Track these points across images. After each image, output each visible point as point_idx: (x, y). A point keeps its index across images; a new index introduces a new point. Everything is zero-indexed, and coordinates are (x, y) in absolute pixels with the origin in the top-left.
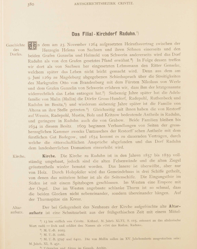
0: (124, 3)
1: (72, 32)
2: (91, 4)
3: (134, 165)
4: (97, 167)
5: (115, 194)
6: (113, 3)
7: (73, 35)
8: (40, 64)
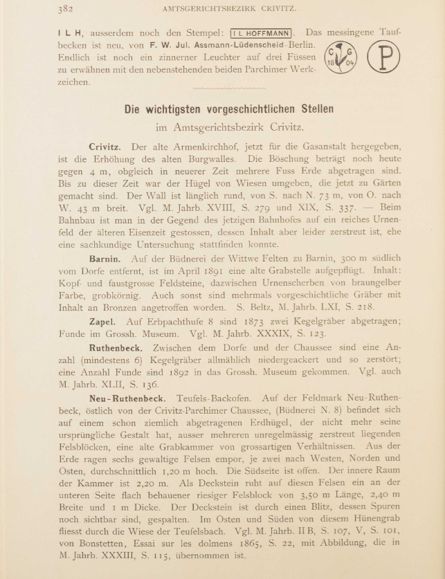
0: (275, 9)
1: (126, 106)
2: (201, 9)
3: (102, 219)
4: (211, 308)
5: (187, 296)
6: (250, 9)
7: (128, 111)
8: (287, 502)
